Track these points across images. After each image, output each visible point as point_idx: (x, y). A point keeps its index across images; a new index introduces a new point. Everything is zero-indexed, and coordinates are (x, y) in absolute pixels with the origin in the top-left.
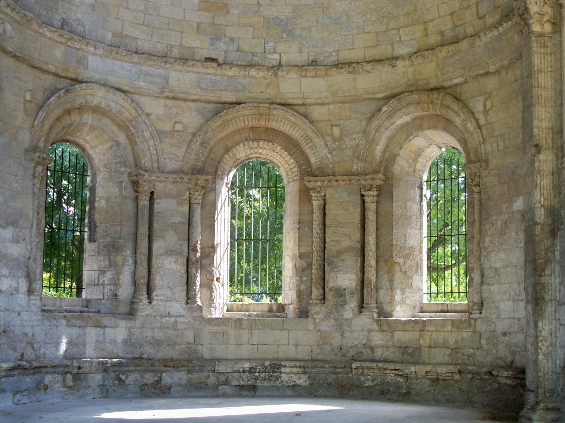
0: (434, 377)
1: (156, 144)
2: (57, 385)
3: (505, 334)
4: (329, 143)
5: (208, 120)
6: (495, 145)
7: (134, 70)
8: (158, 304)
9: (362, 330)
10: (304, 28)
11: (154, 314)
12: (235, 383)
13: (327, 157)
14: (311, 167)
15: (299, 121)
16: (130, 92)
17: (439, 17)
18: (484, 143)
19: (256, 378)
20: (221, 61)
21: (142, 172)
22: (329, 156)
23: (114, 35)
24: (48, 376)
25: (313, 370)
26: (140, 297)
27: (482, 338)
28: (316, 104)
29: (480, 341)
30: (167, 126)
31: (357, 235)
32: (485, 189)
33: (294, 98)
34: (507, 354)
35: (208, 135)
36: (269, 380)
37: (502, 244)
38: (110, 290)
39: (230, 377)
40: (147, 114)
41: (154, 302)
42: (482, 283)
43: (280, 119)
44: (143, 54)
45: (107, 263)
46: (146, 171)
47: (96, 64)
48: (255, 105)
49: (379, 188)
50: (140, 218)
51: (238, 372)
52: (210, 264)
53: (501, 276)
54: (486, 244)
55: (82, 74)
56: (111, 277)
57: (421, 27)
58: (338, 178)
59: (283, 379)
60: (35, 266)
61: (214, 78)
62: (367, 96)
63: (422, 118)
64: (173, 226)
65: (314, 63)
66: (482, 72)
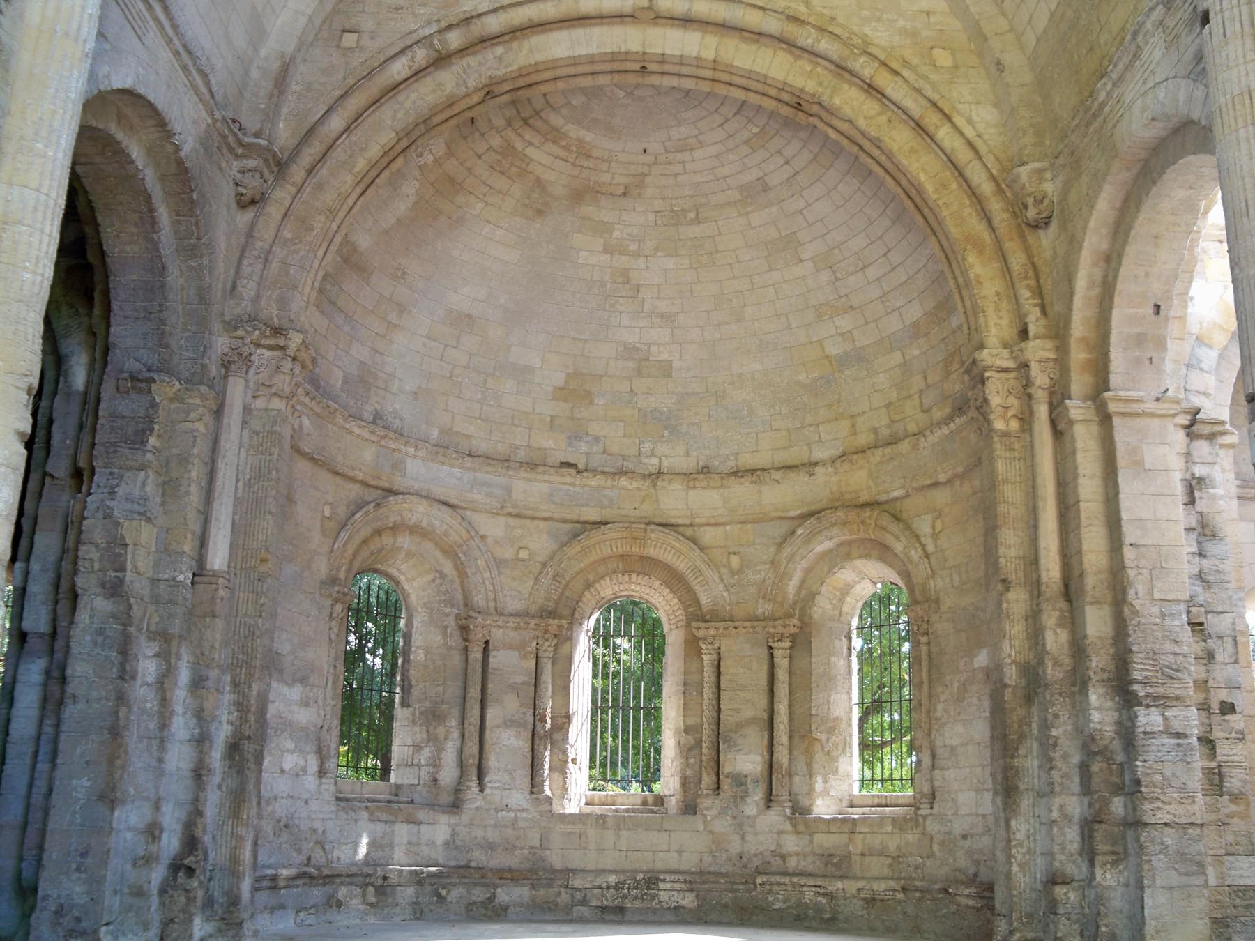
2: (354, 901)
3: (965, 837)
5: (563, 545)
6: (947, 580)
9: (770, 832)
10: (693, 424)
12: (594, 903)
17: (871, 409)
19: (625, 897)
20: (581, 466)
21: (474, 615)
22: (725, 594)
23: (442, 432)
28: (708, 525)
30: (508, 553)
31: (763, 702)
41: (487, 791)
42: (933, 767)
45: (425, 736)
47: (418, 470)
49: (793, 638)
50: (470, 677)
54: (938, 714)
57: (846, 423)
64: (514, 688)
65: (705, 470)
66: (929, 482)
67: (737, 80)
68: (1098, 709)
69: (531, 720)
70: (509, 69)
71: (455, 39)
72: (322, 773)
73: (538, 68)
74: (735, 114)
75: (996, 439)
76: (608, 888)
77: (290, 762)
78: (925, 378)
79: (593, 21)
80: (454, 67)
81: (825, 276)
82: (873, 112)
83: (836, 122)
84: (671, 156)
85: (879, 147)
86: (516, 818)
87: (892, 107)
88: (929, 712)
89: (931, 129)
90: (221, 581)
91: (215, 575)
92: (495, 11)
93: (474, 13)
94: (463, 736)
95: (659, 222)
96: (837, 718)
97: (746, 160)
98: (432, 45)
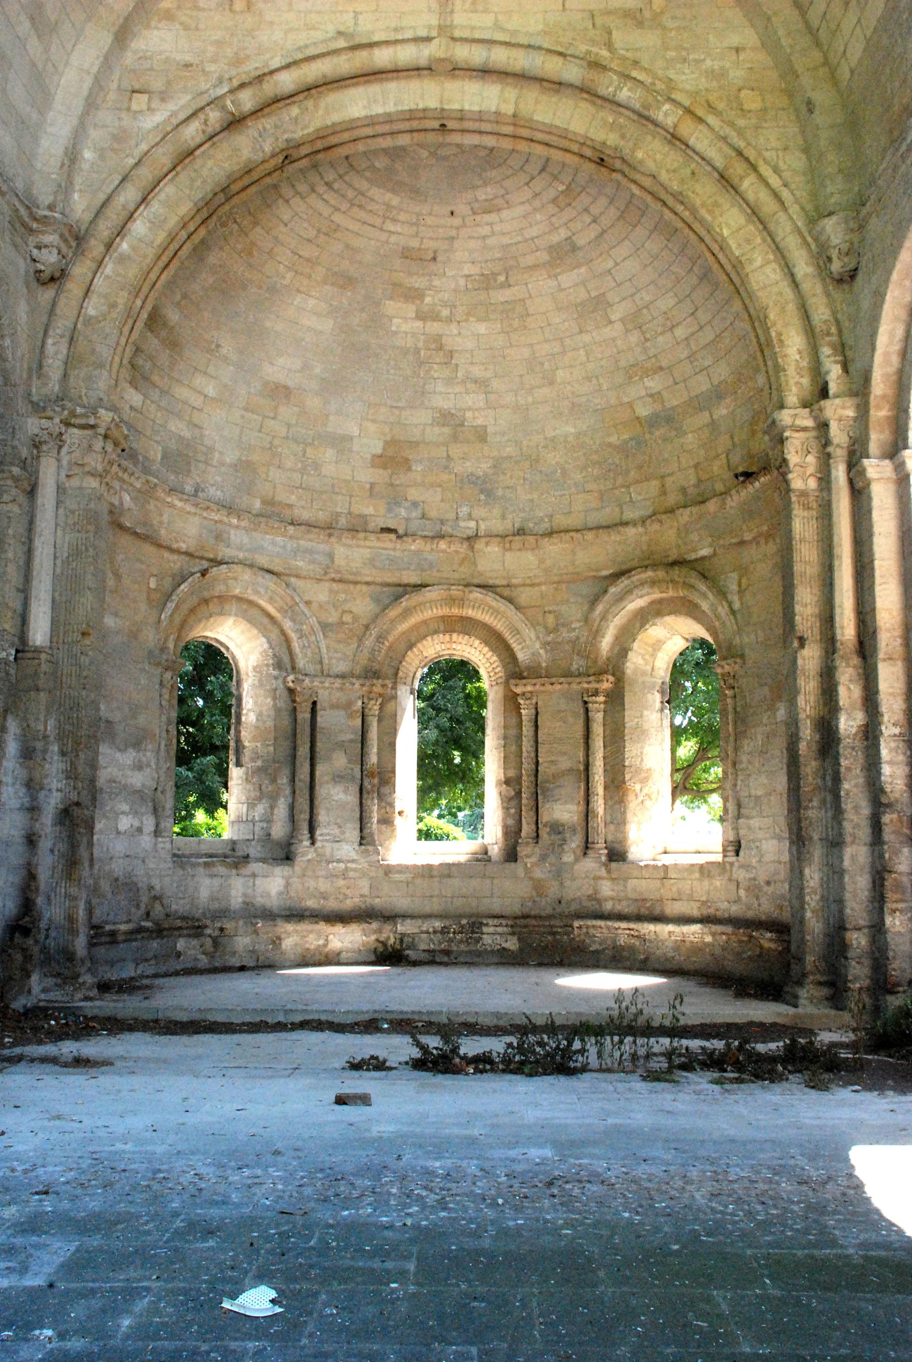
3: (768, 883)
6: (753, 636)
15: (502, 605)
19: (451, 940)
20: (401, 532)
21: (301, 677)
23: (265, 502)
31: (581, 755)
41: (318, 844)
42: (739, 816)
46: (306, 675)
47: (240, 539)
48: (445, 587)
50: (299, 736)
51: (428, 932)
54: (744, 766)
55: (224, 552)
57: (655, 483)
58: (554, 680)
63: (660, 601)
65: (521, 532)
67: (539, 136)
68: (889, 763)
69: (358, 775)
70: (306, 132)
71: (247, 100)
72: (157, 833)
73: (335, 129)
74: (540, 173)
75: (794, 499)
76: (435, 932)
77: (125, 823)
78: (732, 438)
79: (390, 75)
80: (250, 132)
81: (634, 337)
82: (676, 165)
83: (638, 177)
84: (478, 218)
85: (682, 203)
86: (347, 868)
87: (696, 158)
89: (735, 181)
90: (43, 656)
91: (38, 650)
92: (288, 66)
93: (266, 70)
94: (294, 792)
95: (469, 286)
96: (649, 770)
97: (554, 219)
98: (224, 108)
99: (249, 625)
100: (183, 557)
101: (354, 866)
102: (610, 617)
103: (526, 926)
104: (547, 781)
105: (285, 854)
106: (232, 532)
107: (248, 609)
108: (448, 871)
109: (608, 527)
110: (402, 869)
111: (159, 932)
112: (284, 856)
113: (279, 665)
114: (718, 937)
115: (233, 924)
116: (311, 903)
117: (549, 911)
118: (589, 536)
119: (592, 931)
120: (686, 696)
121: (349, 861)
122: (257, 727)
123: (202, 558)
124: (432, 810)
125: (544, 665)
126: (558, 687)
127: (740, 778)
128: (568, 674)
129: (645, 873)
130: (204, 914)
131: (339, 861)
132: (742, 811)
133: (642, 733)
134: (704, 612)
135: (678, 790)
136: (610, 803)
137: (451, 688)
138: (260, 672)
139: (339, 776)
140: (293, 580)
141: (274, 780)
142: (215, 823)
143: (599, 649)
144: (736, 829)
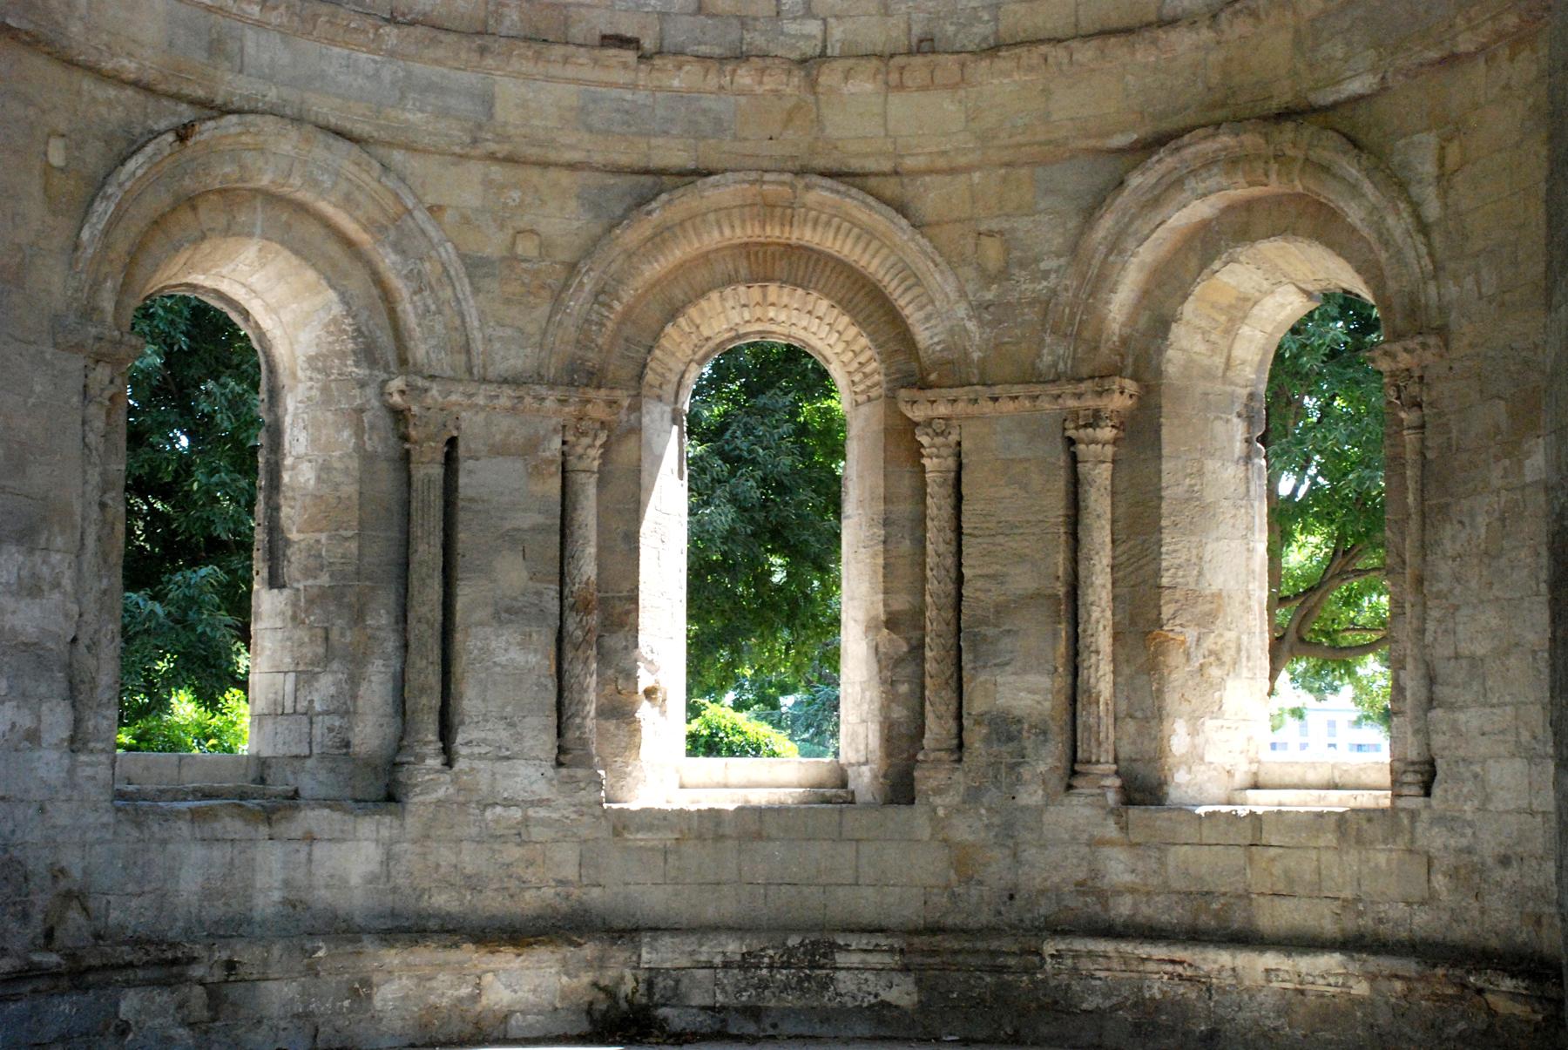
0: (1288, 985)
1: (460, 296)
3: (1505, 861)
4: (970, 288)
6: (1469, 282)
7: (386, 75)
8: (472, 769)
11: (461, 799)
13: (965, 330)
14: (918, 359)
16: (377, 142)
18: (1435, 277)
19: (763, 985)
20: (648, 44)
21: (420, 382)
24: (131, 993)
25: (931, 961)
26: (418, 750)
27: (1433, 869)
28: (931, 171)
29: (1429, 881)
30: (493, 244)
31: (1061, 559)
32: (1440, 415)
33: (867, 155)
34: (1516, 923)
35: (614, 267)
36: (802, 989)
37: (1491, 584)
38: (330, 730)
39: (685, 981)
40: (430, 209)
41: (461, 764)
42: (1430, 703)
43: (824, 217)
44: (412, 23)
45: (321, 650)
46: (432, 377)
48: (753, 176)
50: (416, 517)
51: (710, 966)
52: (626, 648)
53: (1489, 683)
54: (1442, 586)
55: (231, 85)
56: (332, 690)
58: (997, 390)
59: (842, 988)
60: (92, 663)
61: (629, 96)
62: (1083, 144)
63: (1249, 205)
64: (513, 539)
65: (926, 46)
66: (1434, 54)
69: (554, 607)
72: (76, 742)
86: (526, 820)
88: (1420, 581)
96: (1218, 595)
99: (295, 261)
100: (130, 92)
101: (543, 813)
102: (1130, 244)
103: (934, 953)
104: (984, 621)
105: (384, 788)
106: (250, 36)
107: (292, 223)
108: (754, 824)
109: (1128, 31)
110: (653, 819)
111: (76, 976)
112: (383, 793)
113: (368, 354)
114: (1383, 985)
115: (258, 951)
116: (443, 901)
117: (985, 917)
118: (1086, 53)
119: (1086, 965)
120: (1308, 429)
121: (532, 804)
122: (318, 498)
123: (177, 97)
124: (722, 689)
125: (976, 355)
126: (1007, 407)
127: (1435, 614)
128: (1032, 377)
129: (1208, 834)
130: (187, 931)
131: (508, 803)
132: (1438, 689)
133: (1201, 512)
134: (1353, 230)
135: (1282, 648)
136: (1126, 670)
137: (764, 412)
138: (326, 371)
139: (508, 610)
140: (397, 156)
141: (358, 617)
142: (217, 721)
143: (1103, 320)
144: (1424, 732)
